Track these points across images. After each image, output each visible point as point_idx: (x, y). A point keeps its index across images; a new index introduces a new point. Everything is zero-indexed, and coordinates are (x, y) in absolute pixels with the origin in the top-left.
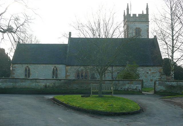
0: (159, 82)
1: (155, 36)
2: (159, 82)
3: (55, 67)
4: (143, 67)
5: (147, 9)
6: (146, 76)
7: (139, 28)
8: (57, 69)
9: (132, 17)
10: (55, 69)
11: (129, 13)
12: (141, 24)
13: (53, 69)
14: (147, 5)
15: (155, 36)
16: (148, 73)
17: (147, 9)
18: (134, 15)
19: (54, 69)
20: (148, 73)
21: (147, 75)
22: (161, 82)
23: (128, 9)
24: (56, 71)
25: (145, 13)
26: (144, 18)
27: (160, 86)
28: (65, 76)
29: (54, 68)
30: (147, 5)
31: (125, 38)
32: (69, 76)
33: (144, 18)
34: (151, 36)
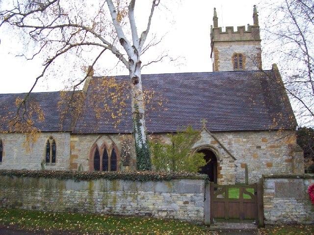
0: (276, 184)
1: (274, 65)
2: (279, 180)
3: (51, 138)
4: (247, 134)
5: (255, 16)
6: (255, 156)
7: (240, 55)
8: (54, 143)
9: (224, 33)
10: (51, 141)
11: (219, 26)
12: (245, 46)
13: (46, 142)
14: (215, 12)
15: (274, 65)
16: (259, 147)
17: (255, 16)
18: (230, 29)
19: (48, 143)
20: (259, 147)
21: (259, 152)
22: (286, 181)
23: (215, 19)
24: (53, 146)
25: (252, 24)
26: (253, 33)
27: (282, 197)
28: (69, 157)
29: (48, 141)
30: (215, 12)
31: (215, 74)
32: (76, 156)
33: (253, 33)
34: (267, 66)
